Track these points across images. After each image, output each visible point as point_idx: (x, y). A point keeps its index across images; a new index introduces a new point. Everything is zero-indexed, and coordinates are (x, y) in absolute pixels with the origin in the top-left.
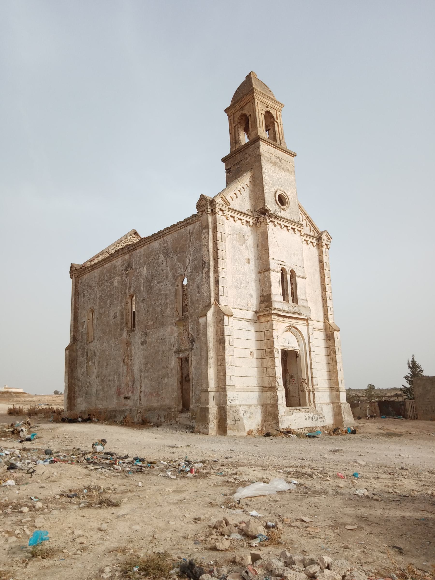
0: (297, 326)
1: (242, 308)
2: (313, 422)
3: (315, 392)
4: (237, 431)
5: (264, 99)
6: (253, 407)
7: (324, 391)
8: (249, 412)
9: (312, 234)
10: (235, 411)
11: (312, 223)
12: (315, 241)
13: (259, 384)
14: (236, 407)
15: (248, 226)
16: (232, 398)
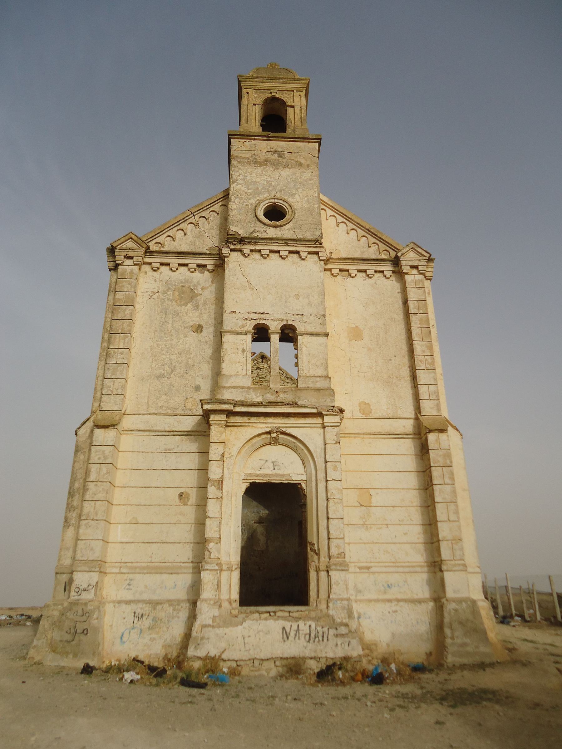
0: (288, 431)
1: (169, 412)
2: (311, 646)
3: (330, 573)
4: (71, 656)
5: (258, 84)
6: (166, 606)
7: (407, 570)
8: (151, 618)
9: (372, 253)
10: (80, 613)
11: (380, 239)
12: (388, 268)
13: (194, 557)
14: (86, 604)
15: (206, 273)
16: (85, 586)
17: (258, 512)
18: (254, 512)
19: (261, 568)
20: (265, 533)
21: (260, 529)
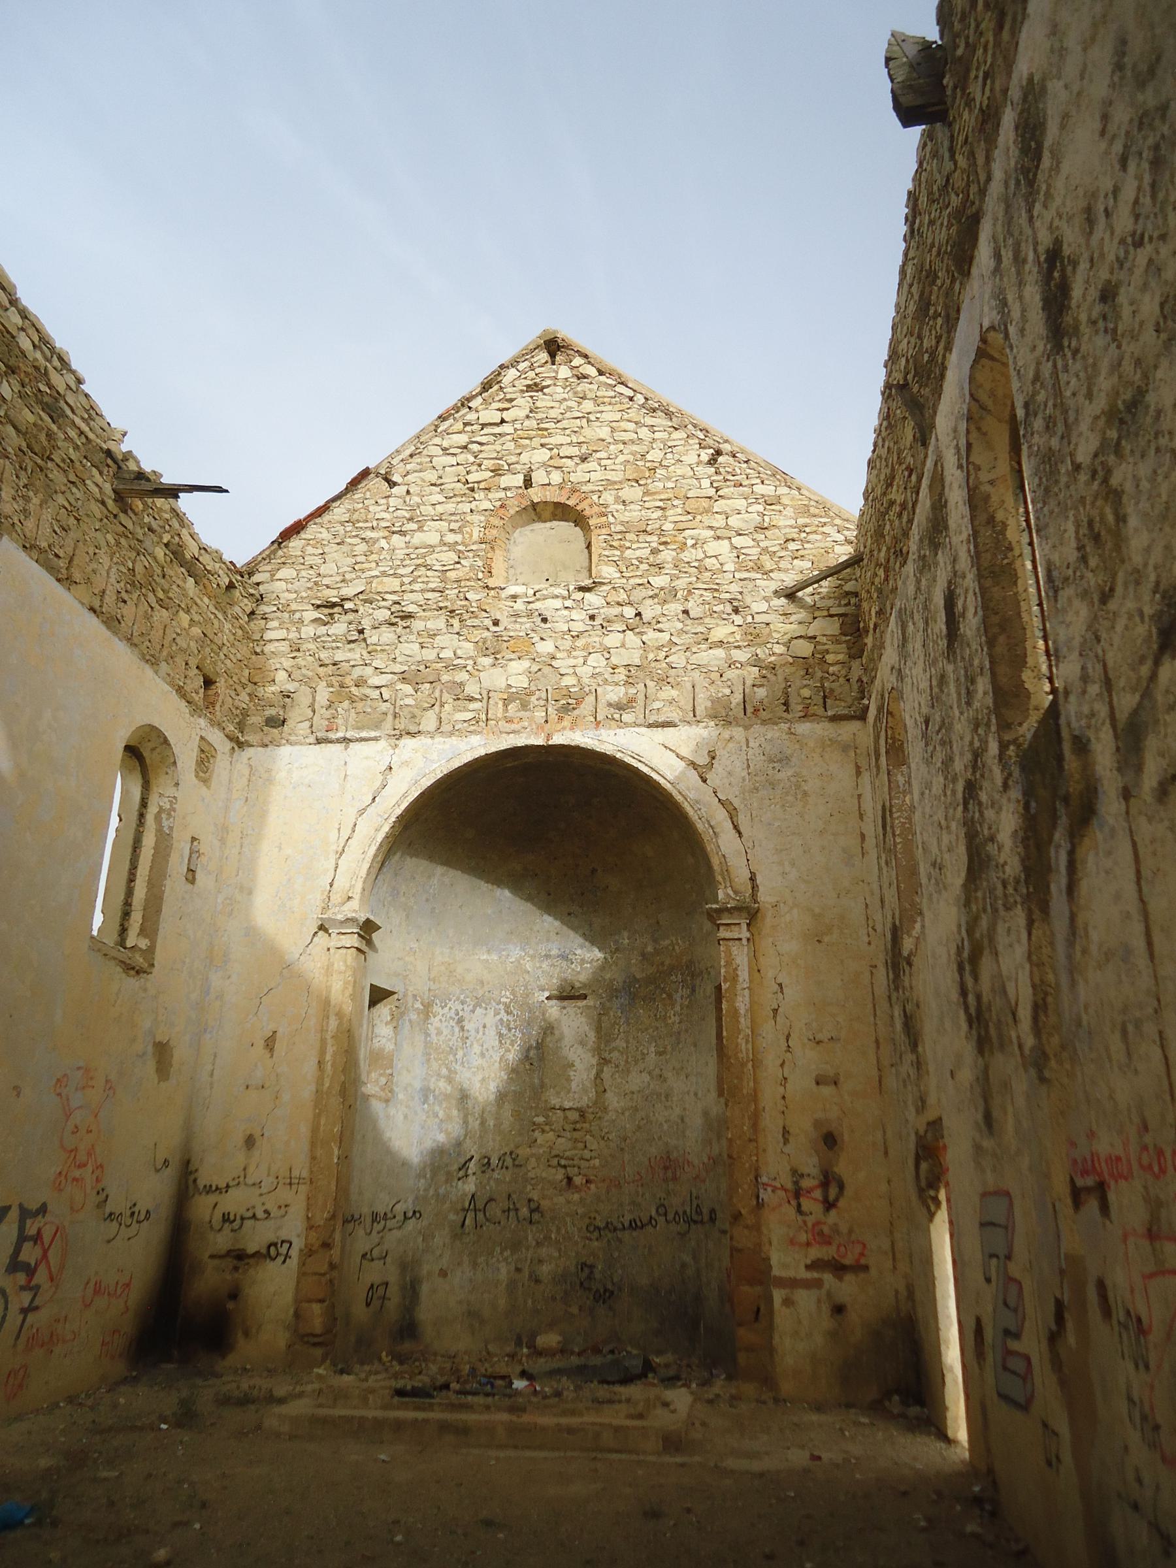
17: (564, 957)
18: (547, 956)
19: (578, 1180)
20: (592, 1035)
21: (573, 1023)
